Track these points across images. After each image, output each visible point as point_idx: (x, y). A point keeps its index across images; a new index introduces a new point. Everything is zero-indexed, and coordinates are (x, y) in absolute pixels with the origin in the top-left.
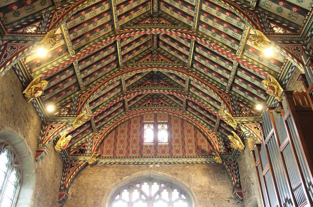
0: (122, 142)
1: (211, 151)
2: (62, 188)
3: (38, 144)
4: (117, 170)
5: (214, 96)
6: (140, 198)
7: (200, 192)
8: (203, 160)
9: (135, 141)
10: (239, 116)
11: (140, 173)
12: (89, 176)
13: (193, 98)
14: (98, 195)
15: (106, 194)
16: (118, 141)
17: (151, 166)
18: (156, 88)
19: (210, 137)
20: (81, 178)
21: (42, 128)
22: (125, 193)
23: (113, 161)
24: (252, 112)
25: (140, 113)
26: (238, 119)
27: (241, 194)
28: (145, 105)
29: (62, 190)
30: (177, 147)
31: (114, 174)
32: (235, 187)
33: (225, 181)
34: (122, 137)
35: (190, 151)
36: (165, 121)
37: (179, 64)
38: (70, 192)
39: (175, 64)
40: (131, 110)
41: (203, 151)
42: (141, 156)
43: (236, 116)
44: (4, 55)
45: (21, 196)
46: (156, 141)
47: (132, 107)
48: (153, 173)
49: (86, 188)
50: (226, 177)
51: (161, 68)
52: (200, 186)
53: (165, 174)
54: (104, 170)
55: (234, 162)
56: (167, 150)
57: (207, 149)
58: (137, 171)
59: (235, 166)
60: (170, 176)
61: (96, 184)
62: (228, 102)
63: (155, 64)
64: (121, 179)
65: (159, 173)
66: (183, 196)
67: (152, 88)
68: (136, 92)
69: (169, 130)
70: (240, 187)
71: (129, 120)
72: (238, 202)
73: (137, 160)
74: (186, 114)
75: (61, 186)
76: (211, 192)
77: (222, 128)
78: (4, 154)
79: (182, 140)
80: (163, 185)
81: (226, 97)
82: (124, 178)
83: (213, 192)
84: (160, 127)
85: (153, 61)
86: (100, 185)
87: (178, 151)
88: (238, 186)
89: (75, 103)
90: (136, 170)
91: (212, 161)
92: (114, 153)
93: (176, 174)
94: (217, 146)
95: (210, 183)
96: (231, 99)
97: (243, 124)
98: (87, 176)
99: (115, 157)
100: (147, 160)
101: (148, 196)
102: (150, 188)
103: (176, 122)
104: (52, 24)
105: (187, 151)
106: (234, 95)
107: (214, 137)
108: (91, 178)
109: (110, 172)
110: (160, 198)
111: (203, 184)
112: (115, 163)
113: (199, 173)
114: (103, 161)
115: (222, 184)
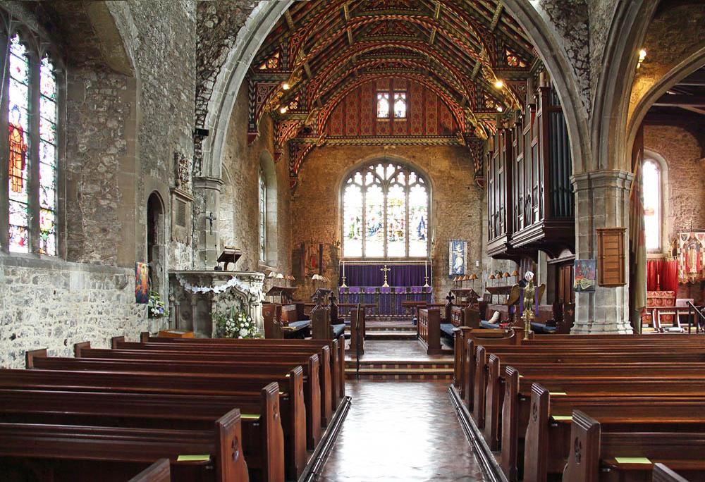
2: (292, 175)
3: (274, 145)
4: (348, 152)
5: (475, 34)
6: (374, 182)
7: (439, 178)
8: (446, 141)
11: (374, 155)
12: (318, 160)
13: (445, 31)
14: (330, 181)
15: (338, 180)
16: (348, 116)
17: (386, 147)
18: (391, 56)
21: (274, 127)
22: (358, 177)
23: (343, 141)
24: (366, 334)
25: (372, 79)
26: (479, 115)
28: (377, 33)
29: (252, 129)
30: (416, 124)
34: (351, 111)
36: (404, 90)
37: (419, 39)
39: (414, 39)
40: (358, 42)
41: (446, 130)
42: (374, 136)
45: (268, 197)
46: (391, 114)
47: (356, 11)
48: (388, 155)
49: (316, 172)
51: (398, 44)
52: (440, 171)
53: (403, 157)
54: (334, 152)
57: (451, 127)
58: (370, 154)
59: (480, 150)
60: (407, 159)
61: (327, 168)
63: (390, 38)
64: (353, 162)
65: (396, 155)
66: (421, 180)
67: (387, 56)
68: (368, 62)
69: (407, 101)
71: (360, 88)
73: (370, 141)
74: (430, 81)
75: (291, 172)
76: (451, 178)
77: (504, 24)
79: (423, 115)
80: (399, 167)
81: (470, 86)
82: (357, 162)
83: (453, 178)
85: (389, 7)
86: (331, 169)
88: (480, 173)
89: (304, 95)
90: (370, 152)
92: (344, 131)
93: (414, 157)
95: (451, 168)
98: (315, 159)
99: (345, 137)
100: (381, 141)
101: (383, 179)
102: (385, 171)
103: (416, 90)
104: (292, 57)
106: (480, 84)
108: (322, 162)
110: (396, 182)
111: (443, 169)
112: (345, 144)
113: (439, 156)
114: (332, 142)
115: (464, 169)
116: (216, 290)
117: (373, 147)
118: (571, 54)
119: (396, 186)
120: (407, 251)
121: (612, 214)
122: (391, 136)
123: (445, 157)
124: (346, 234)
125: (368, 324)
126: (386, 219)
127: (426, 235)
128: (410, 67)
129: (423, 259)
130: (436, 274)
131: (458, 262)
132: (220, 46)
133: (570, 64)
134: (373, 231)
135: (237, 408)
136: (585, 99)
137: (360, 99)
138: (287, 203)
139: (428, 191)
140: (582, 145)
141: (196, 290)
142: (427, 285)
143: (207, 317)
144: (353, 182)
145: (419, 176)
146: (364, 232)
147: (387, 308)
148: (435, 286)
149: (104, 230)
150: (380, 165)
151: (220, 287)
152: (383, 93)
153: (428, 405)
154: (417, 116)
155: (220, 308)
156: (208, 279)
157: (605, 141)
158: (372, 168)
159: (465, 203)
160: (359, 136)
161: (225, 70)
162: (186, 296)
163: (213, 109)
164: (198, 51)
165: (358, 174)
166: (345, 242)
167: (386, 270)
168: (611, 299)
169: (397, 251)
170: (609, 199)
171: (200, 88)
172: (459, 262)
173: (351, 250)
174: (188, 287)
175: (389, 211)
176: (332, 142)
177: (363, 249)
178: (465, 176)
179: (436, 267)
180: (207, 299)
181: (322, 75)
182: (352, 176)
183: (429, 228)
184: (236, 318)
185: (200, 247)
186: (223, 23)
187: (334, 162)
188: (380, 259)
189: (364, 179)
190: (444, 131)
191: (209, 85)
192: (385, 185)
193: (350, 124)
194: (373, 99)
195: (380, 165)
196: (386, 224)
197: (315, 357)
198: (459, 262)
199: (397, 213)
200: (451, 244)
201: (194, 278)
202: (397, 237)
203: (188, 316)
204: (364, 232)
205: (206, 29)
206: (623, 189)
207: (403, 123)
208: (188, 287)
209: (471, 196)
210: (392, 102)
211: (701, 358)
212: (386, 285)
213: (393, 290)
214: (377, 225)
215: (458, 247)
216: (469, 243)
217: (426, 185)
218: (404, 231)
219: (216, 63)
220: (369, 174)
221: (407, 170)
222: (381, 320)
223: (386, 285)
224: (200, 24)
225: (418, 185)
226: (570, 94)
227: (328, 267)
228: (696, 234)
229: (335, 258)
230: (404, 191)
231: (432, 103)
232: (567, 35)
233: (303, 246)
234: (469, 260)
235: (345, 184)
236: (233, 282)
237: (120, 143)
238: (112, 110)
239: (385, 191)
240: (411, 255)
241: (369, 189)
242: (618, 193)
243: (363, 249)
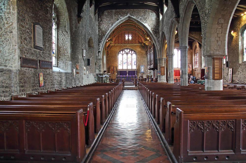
0: (120, 39)
6: (125, 53)
8: (140, 45)
9: (123, 40)
14: (115, 53)
16: (119, 39)
20: (111, 49)
22: (121, 52)
23: (118, 45)
26: (146, 41)
30: (134, 41)
31: (119, 48)
34: (120, 38)
35: (137, 42)
38: (109, 52)
41: (140, 42)
48: (128, 48)
52: (139, 51)
56: (131, 42)
57: (141, 42)
66: (135, 53)
69: (132, 36)
76: (141, 52)
78: (245, 60)
80: (130, 50)
84: (129, 35)
87: (134, 42)
99: (119, 44)
100: (126, 45)
105: (136, 42)
108: (113, 49)
109: (118, 48)
110: (129, 53)
114: (116, 45)
116: (104, 76)
117: (124, 46)
118: (157, 39)
119: (129, 54)
120: (132, 68)
121: (163, 64)
122: (128, 44)
123: (140, 48)
124: (119, 64)
125: (125, 83)
126: (127, 61)
127: (136, 64)
128: (133, 25)
129: (136, 69)
130: (138, 72)
131: (142, 70)
132: (102, 38)
133: (156, 41)
134: (125, 63)
135: (98, 98)
136: (159, 46)
137: (122, 36)
138: (107, 58)
139: (136, 55)
140: (158, 53)
141: (101, 76)
142: (136, 75)
143: (102, 80)
144: (120, 53)
145: (134, 52)
146: (123, 64)
147: (128, 80)
148: (138, 75)
149: (91, 68)
150: (126, 49)
151: (104, 76)
152: (127, 34)
153: (136, 100)
154: (134, 39)
155: (104, 79)
156: (102, 75)
157: (161, 53)
158: (124, 50)
159: (144, 57)
160: (122, 44)
161: (103, 42)
162: (99, 77)
163: (101, 48)
164: (98, 39)
165: (121, 51)
166: (119, 66)
167: (127, 72)
168: (163, 77)
169: (130, 68)
170: (162, 62)
171: (99, 45)
172: (143, 70)
173: (120, 68)
174: (99, 76)
175: (128, 59)
176: (116, 45)
177: (123, 67)
178: (144, 52)
179: (138, 71)
180: (102, 78)
181: (115, 33)
182: (120, 52)
183: (136, 63)
184: (106, 80)
185: (99, 70)
186: (102, 34)
187: (117, 49)
188: (126, 69)
189: (123, 52)
190: (139, 43)
191: (100, 44)
192: (127, 54)
193: (120, 41)
194: (124, 36)
195: (126, 49)
196: (127, 62)
197: (98, 99)
198: (143, 70)
199: (129, 60)
200: (141, 66)
201: (100, 75)
202: (130, 65)
203: (99, 80)
204: (123, 64)
205: (100, 35)
206: (165, 60)
207: (131, 41)
208: (99, 76)
209: (145, 56)
210: (128, 36)
211: (244, 98)
212: (127, 75)
213: (129, 76)
214: (125, 62)
215: (142, 67)
216: (145, 66)
217: (136, 54)
218: (131, 63)
219: (101, 40)
220: (124, 51)
221: (132, 50)
222: (127, 82)
223: (127, 75)
224: (99, 34)
225: (134, 54)
226: (157, 45)
227: (115, 71)
228: (189, 65)
229: (117, 69)
230: (131, 55)
231: (137, 37)
232: (156, 36)
233: (110, 67)
234: (145, 70)
235: (119, 54)
236: (106, 75)
237: (92, 57)
238: (91, 52)
239: (127, 55)
240: (133, 68)
241: (124, 54)
242: (164, 61)
243: (123, 67)
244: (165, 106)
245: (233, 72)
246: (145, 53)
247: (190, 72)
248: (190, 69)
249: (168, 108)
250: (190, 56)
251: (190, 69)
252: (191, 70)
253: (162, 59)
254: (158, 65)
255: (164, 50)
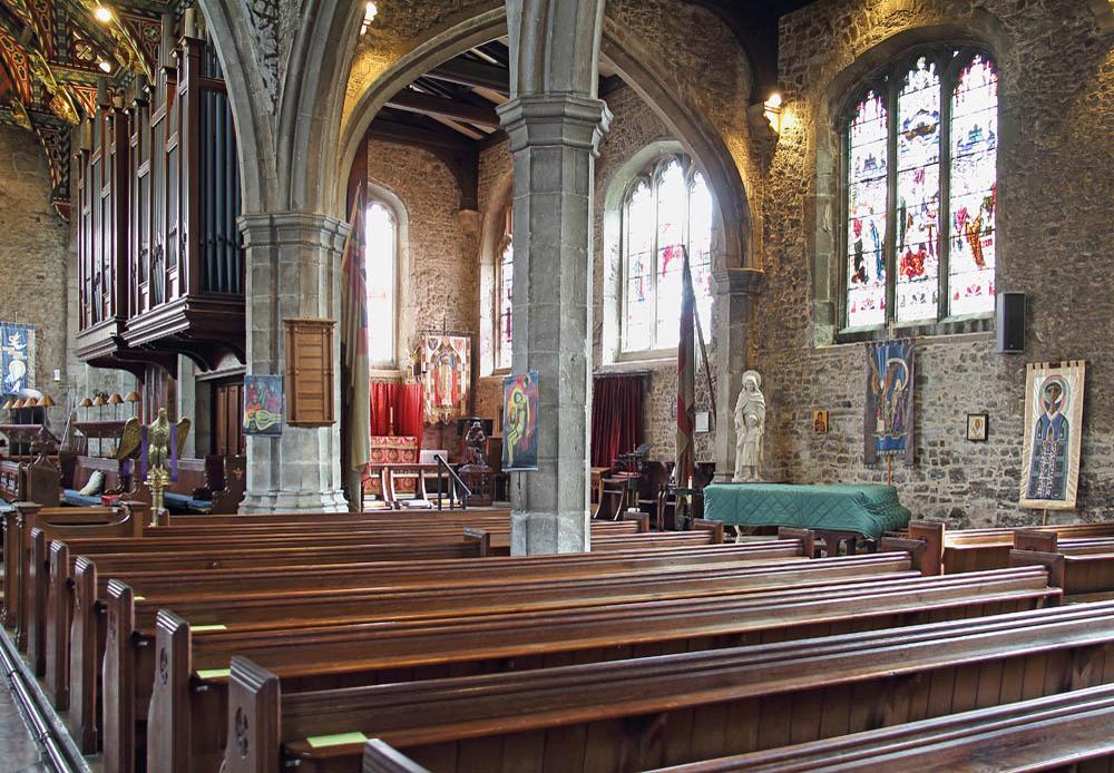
1: (8, 92)
10: (65, 66)
19: (7, 55)
26: (62, 73)
27: (66, 211)
32: (55, 193)
33: (34, 173)
43: (58, 64)
44: (358, 738)
50: (40, 164)
55: (62, 134)
59: (62, 144)
62: (45, 22)
70: (68, 194)
72: (60, 225)
88: (63, 191)
91: (9, 120)
94: (25, 85)
96: (54, 15)
97: (72, 85)
107: (19, 58)
121: (310, 294)
136: (268, 74)
140: (261, 161)
157: (301, 158)
168: (309, 449)
170: (305, 265)
209: (43, 237)
216: (39, 333)
228: (452, 339)
242: (322, 256)
244: (136, 637)
245: (1095, 402)
246: (39, 207)
247: (458, 405)
248: (456, 375)
249: (169, 651)
250: (457, 267)
251: (456, 375)
252: (465, 382)
253: (311, 228)
254: (255, 298)
255: (333, 133)
